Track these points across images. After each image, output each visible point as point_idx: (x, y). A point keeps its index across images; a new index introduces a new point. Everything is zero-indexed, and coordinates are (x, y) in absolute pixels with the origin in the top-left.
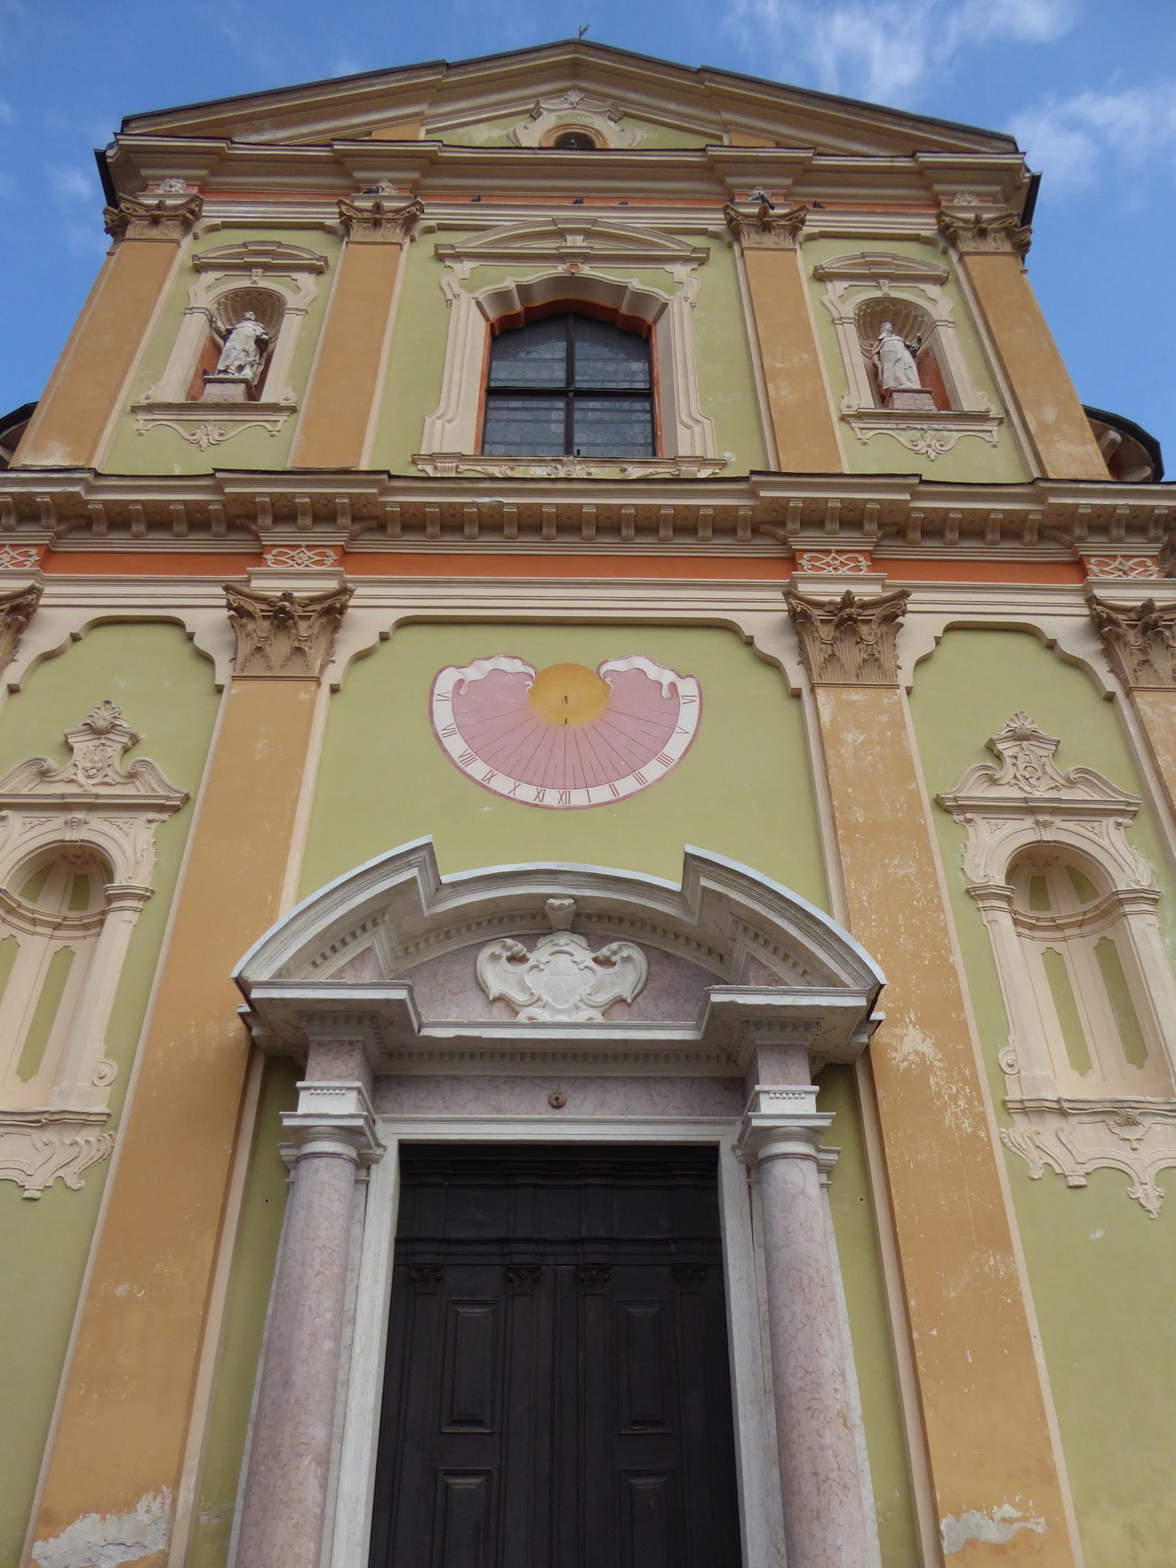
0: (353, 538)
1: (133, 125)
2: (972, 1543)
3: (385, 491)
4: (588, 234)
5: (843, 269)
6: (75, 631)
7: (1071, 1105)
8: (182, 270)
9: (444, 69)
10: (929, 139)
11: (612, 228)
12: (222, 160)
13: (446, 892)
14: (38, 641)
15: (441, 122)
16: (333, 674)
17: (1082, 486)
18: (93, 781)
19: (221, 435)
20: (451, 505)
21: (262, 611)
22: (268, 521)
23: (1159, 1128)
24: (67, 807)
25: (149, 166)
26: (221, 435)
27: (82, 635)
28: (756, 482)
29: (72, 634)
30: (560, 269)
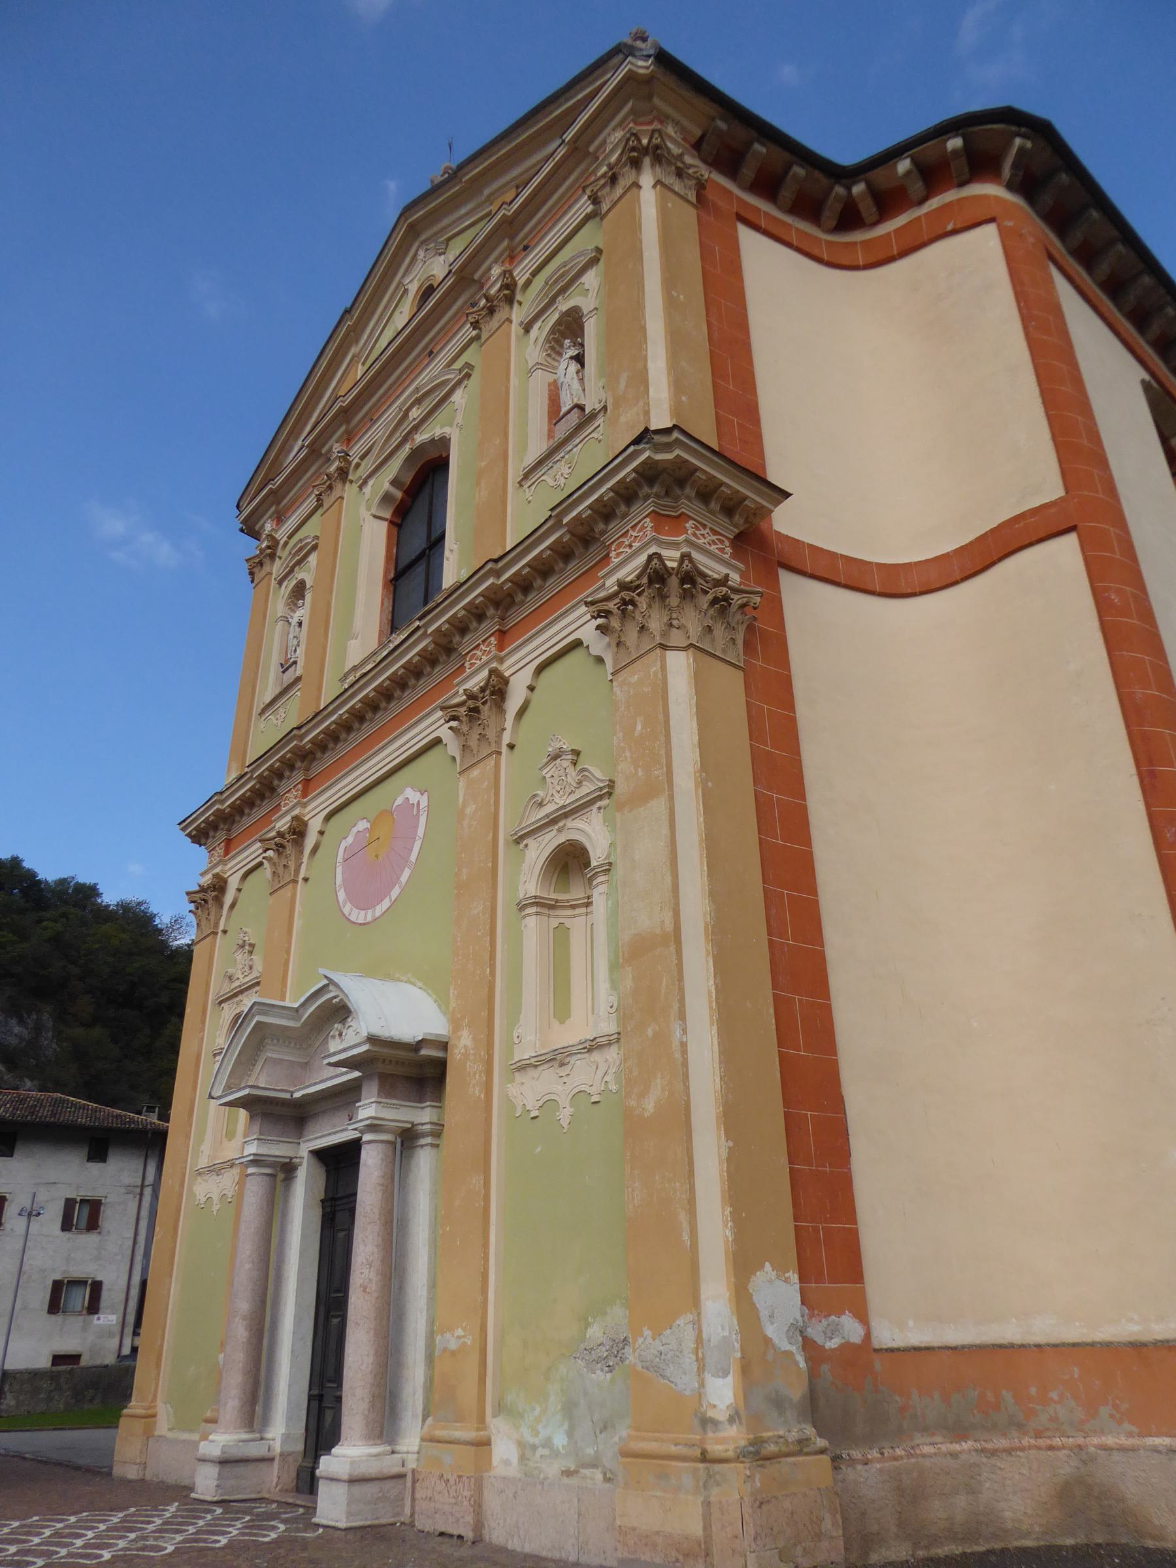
0: (307, 769)
1: (241, 504)
2: (445, 1350)
3: (302, 737)
4: (418, 401)
5: (540, 305)
6: (319, 829)
7: (536, 1059)
8: (517, 336)
9: (347, 316)
10: (578, 101)
11: (429, 385)
12: (275, 493)
13: (301, 1011)
14: (513, 703)
15: (370, 343)
16: (506, 738)
17: (188, 821)
18: (565, 797)
19: (570, 468)
20: (534, 559)
21: (615, 605)
22: (601, 526)
23: (578, 1062)
24: (554, 821)
25: (591, 142)
26: (570, 468)
27: (534, 684)
28: (557, 515)
29: (528, 687)
30: (407, 449)
